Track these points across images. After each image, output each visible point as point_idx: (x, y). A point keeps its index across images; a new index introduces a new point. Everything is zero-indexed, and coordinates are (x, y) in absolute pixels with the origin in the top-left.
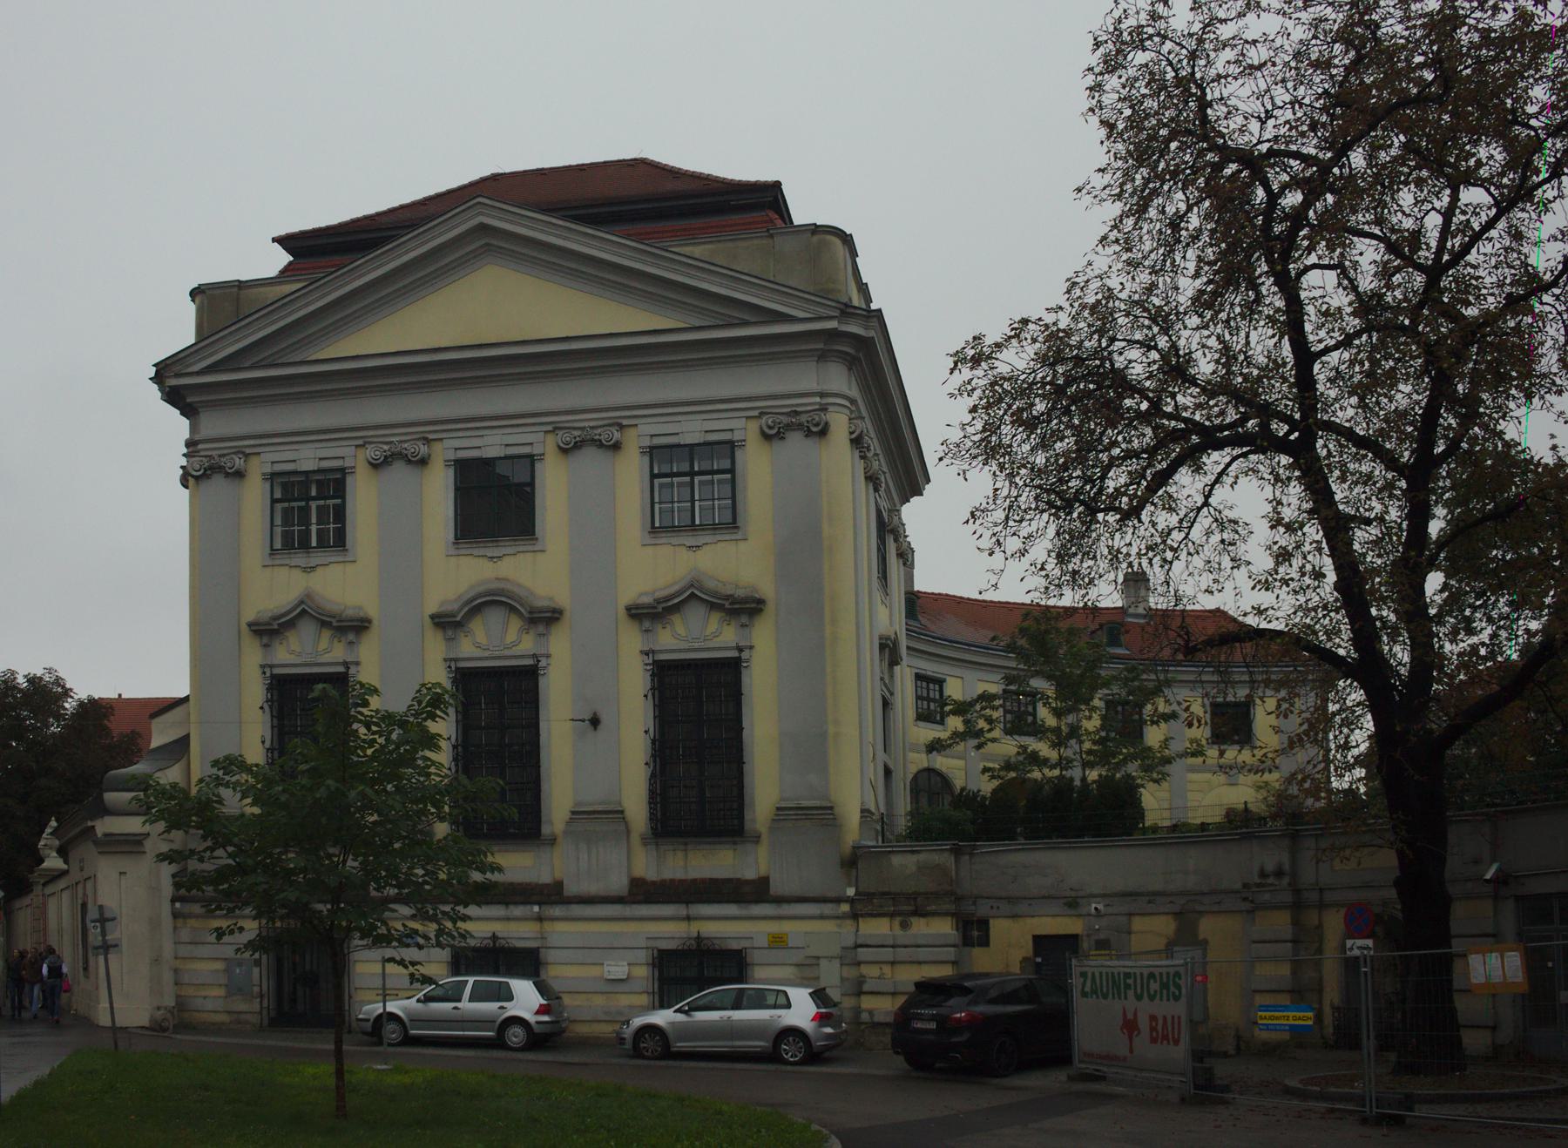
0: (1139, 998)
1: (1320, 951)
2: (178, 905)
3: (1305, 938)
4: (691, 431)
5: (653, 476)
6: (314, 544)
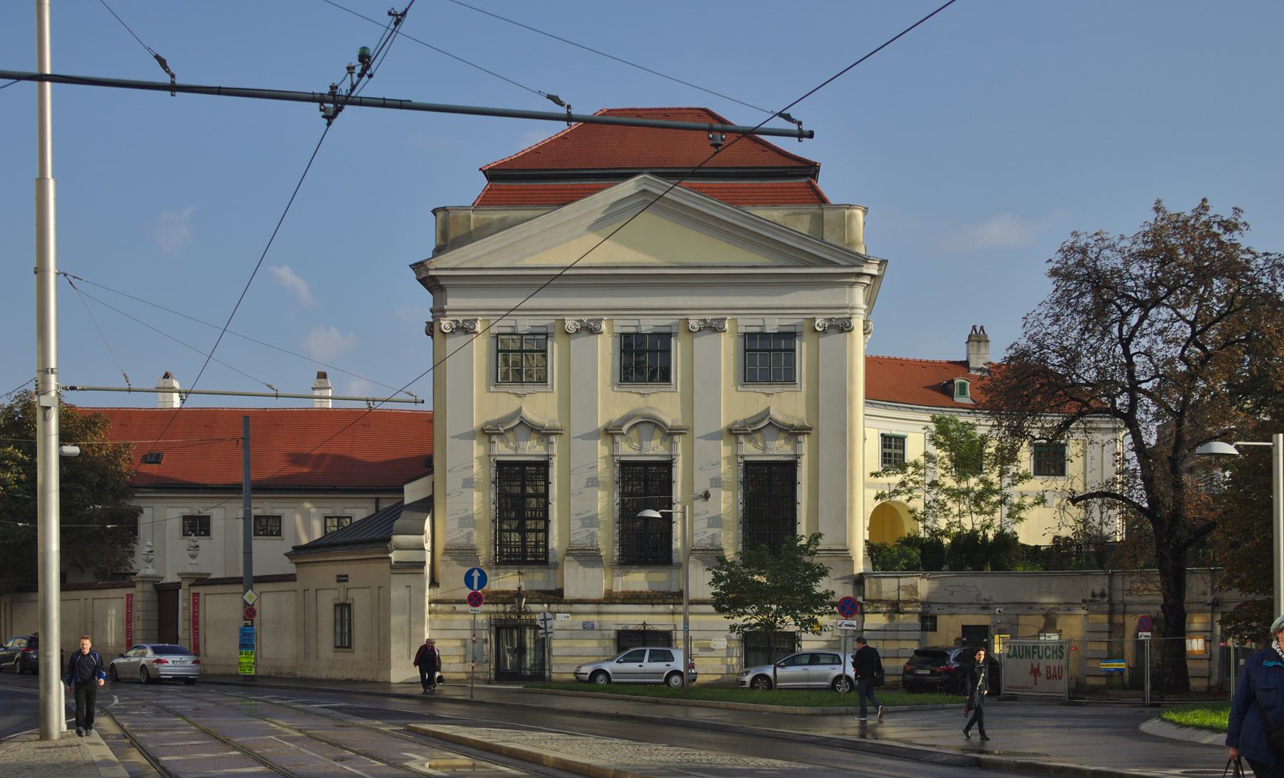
0: (1040, 658)
1: (1123, 637)
3: (1115, 629)
5: (746, 351)
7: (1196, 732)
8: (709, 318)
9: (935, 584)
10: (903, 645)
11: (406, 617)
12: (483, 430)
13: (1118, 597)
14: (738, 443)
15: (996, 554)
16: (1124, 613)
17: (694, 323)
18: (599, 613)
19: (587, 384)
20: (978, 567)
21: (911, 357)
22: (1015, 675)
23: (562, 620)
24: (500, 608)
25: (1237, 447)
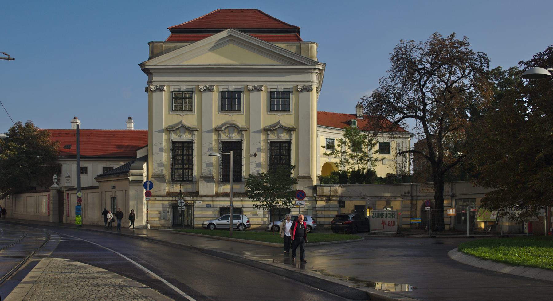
7: (494, 264)
8: (256, 85)
9: (344, 189)
10: (332, 213)
11: (135, 202)
12: (167, 129)
13: (414, 194)
14: (268, 134)
15: (368, 178)
16: (417, 200)
17: (250, 87)
18: (213, 201)
19: (209, 112)
20: (360, 182)
21: (337, 113)
22: (375, 225)
23: (198, 203)
24: (174, 199)
25: (550, 71)
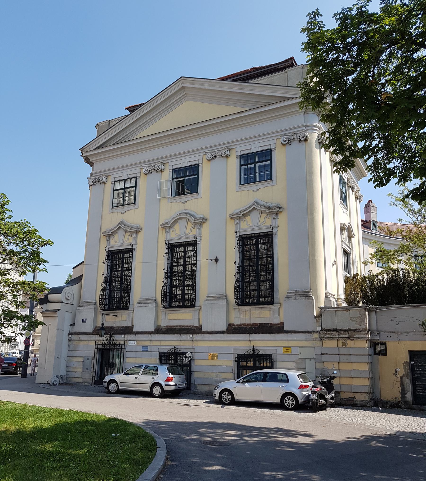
2: (70, 336)
4: (255, 148)
6: (257, 180)
